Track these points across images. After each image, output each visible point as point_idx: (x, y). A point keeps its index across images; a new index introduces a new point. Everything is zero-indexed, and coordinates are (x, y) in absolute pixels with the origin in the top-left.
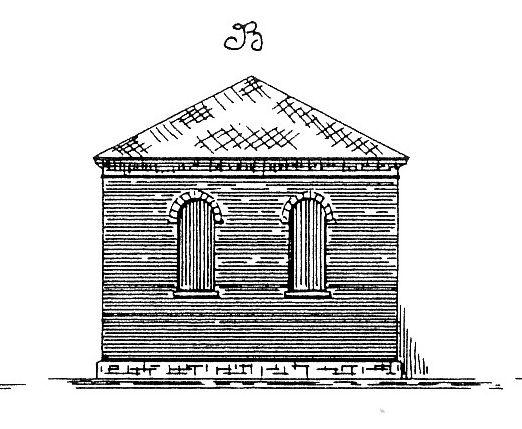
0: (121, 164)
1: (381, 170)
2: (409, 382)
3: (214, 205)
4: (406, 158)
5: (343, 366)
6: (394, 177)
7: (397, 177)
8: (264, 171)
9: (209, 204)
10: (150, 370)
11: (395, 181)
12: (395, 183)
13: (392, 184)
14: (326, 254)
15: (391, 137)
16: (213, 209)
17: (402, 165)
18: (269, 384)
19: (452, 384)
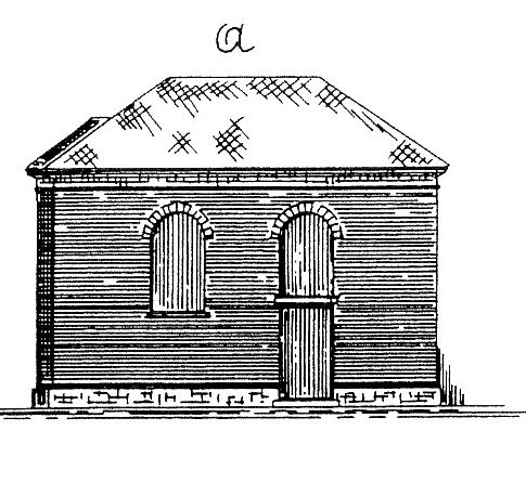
0: (55, 180)
1: (416, 176)
2: (461, 409)
3: (335, 228)
4: (445, 169)
5: (252, 394)
6: (431, 187)
7: (437, 187)
8: (217, 182)
9: (330, 227)
10: (383, 397)
11: (434, 192)
12: (434, 194)
13: (430, 195)
14: (206, 273)
15: (435, 142)
16: (333, 232)
17: (441, 174)
18: (219, 412)
19: (87, 413)
